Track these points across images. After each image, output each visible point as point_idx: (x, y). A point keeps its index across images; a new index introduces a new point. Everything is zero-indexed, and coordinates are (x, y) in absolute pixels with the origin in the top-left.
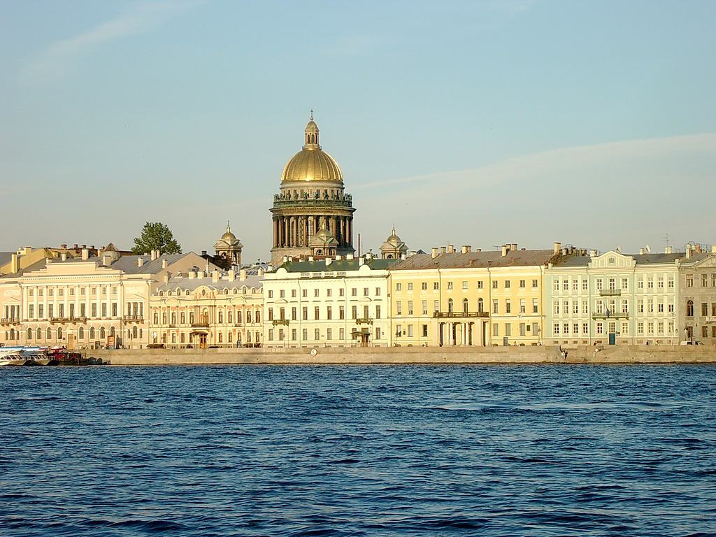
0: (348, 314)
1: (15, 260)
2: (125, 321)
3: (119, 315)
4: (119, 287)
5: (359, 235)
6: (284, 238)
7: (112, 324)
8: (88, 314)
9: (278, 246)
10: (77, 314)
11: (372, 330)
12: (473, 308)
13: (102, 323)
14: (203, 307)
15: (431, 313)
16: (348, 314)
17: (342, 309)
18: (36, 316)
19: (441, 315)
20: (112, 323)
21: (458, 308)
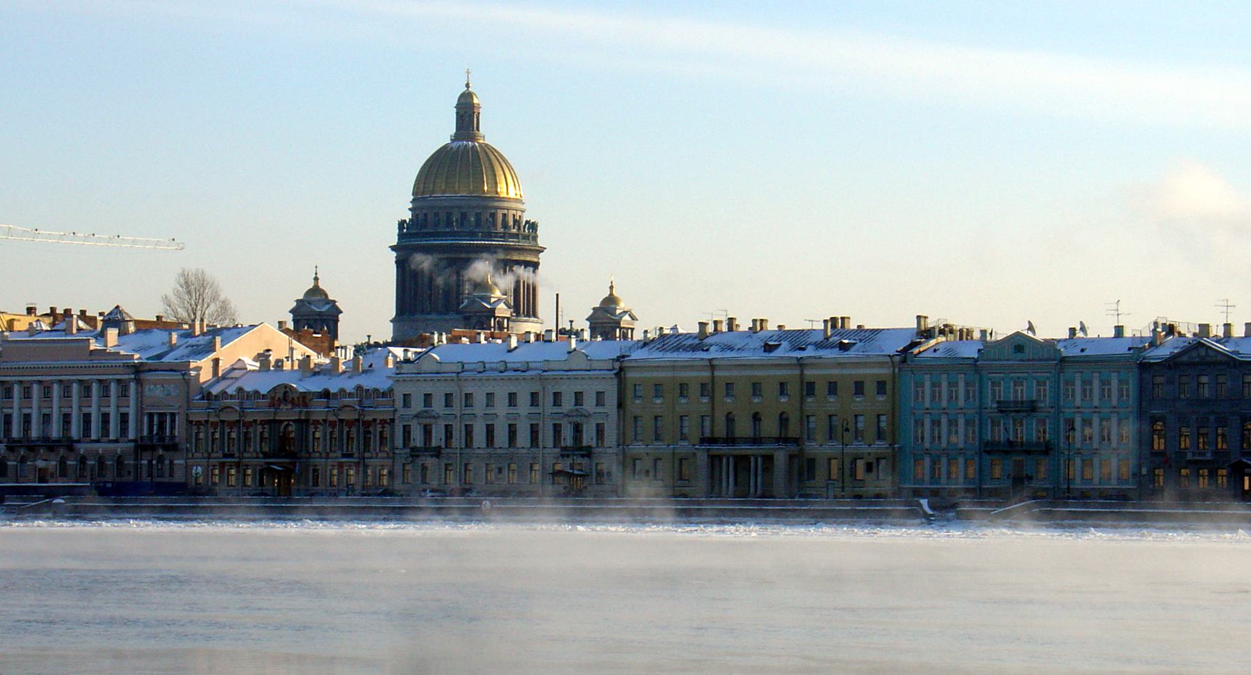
0: (547, 436)
1: (674, 367)
2: (141, 447)
3: (131, 435)
4: (133, 386)
5: (557, 295)
6: (528, 305)
7: (100, 451)
8: (75, 432)
9: (518, 314)
10: (437, 438)
12: (770, 427)
13: (101, 448)
14: (286, 423)
15: (695, 436)
16: (547, 436)
17: (512, 430)
18: (94, 434)
19: (713, 440)
20: (120, 448)
21: (744, 428)
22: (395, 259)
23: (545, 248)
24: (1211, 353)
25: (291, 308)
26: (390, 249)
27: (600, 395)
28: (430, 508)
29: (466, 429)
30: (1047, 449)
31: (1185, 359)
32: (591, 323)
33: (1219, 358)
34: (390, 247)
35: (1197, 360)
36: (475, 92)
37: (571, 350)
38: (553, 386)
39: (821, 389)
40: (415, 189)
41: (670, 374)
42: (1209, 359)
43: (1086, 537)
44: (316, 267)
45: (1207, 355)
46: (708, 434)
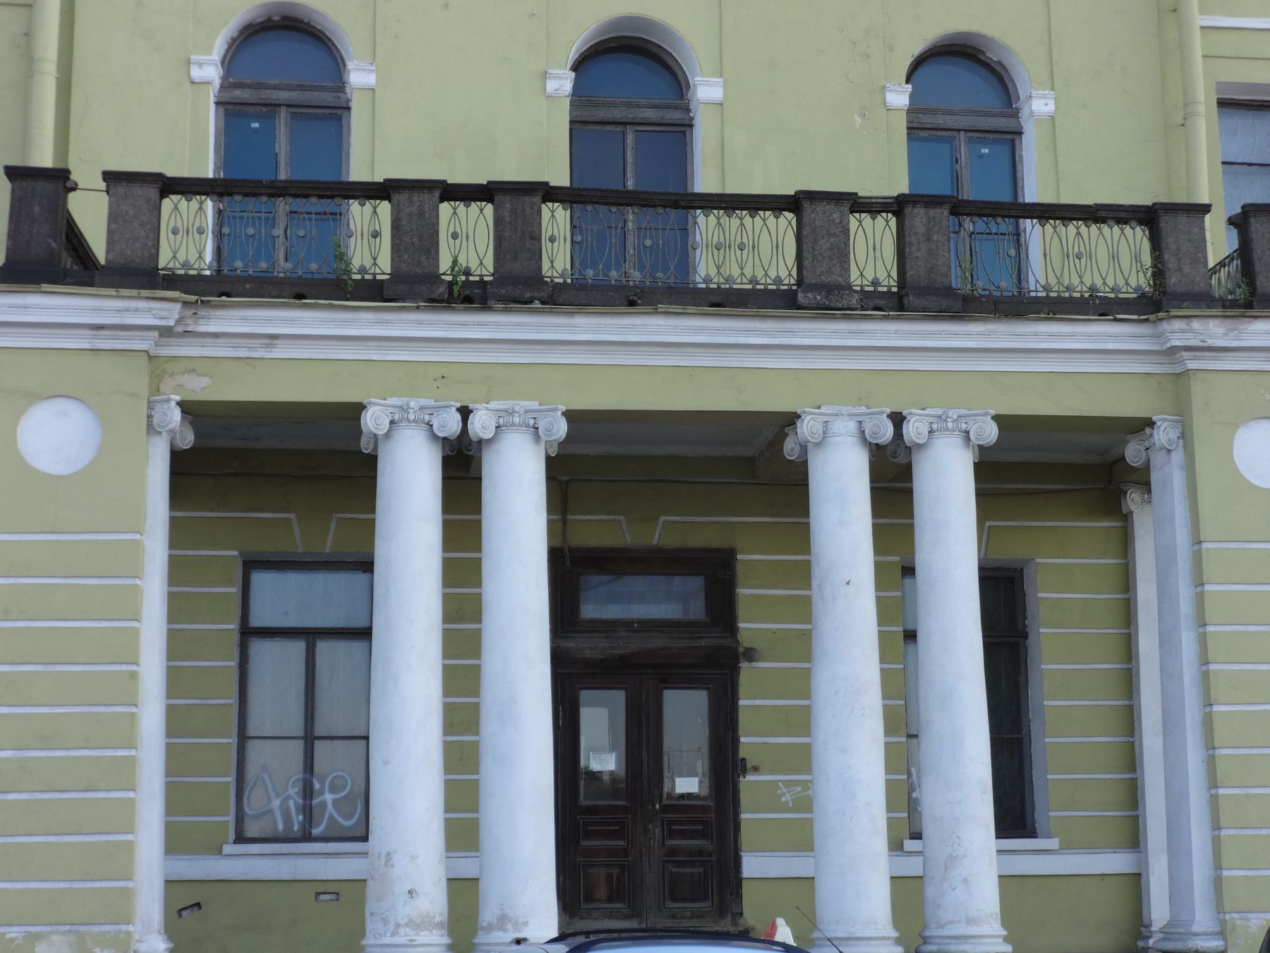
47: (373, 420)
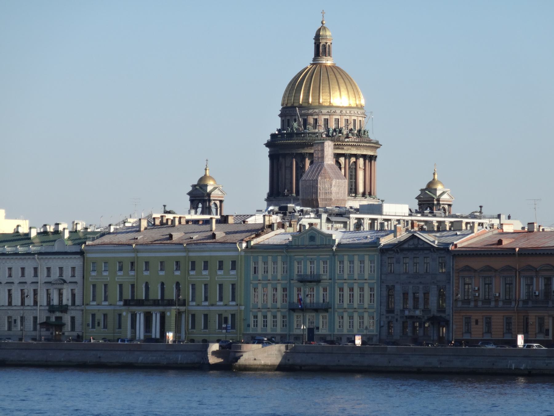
11: (67, 318)
22: (268, 154)
23: (381, 145)
24: (421, 243)
25: (188, 192)
26: (265, 146)
27: (73, 269)
28: (116, 333)
29: (550, 278)
30: (393, 295)
31: (406, 246)
32: (419, 201)
33: (426, 246)
34: (264, 144)
35: (412, 247)
36: (327, 27)
37: (41, 246)
38: (63, 263)
39: (200, 265)
40: (286, 99)
41: (184, 254)
42: (419, 246)
43: (234, 341)
44: (207, 160)
45: (418, 243)
46: (527, 284)
47: (151, 313)
